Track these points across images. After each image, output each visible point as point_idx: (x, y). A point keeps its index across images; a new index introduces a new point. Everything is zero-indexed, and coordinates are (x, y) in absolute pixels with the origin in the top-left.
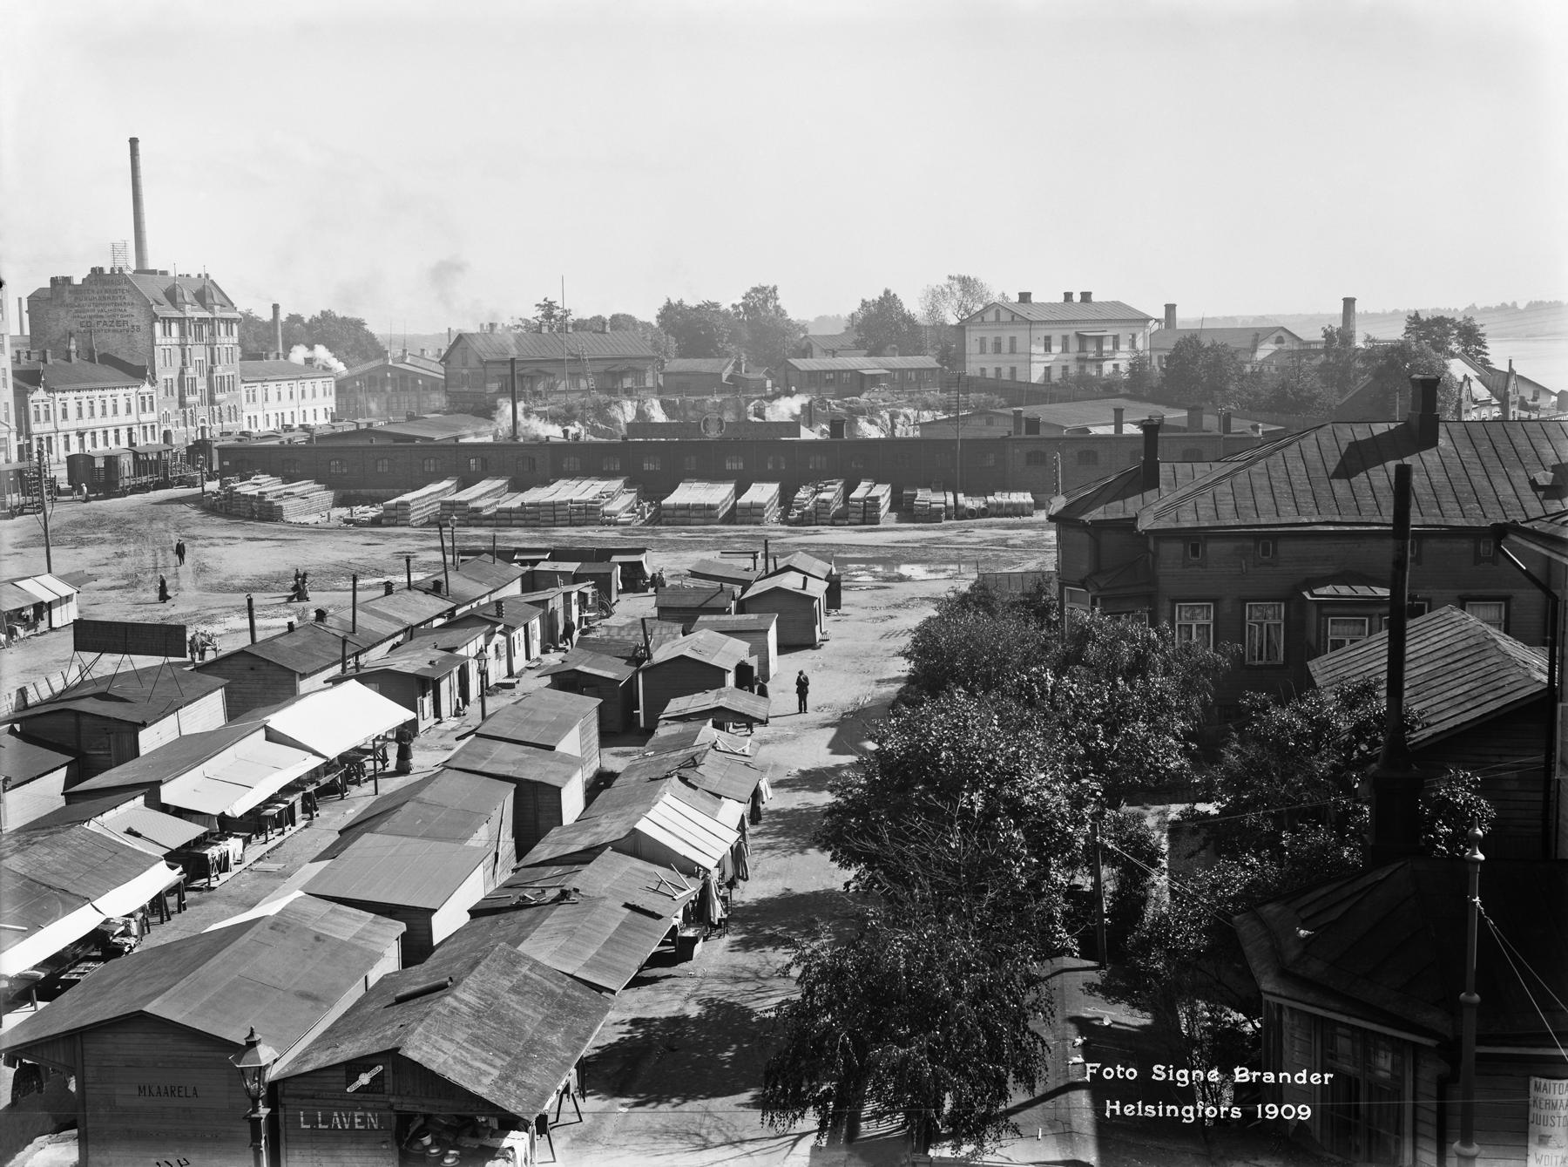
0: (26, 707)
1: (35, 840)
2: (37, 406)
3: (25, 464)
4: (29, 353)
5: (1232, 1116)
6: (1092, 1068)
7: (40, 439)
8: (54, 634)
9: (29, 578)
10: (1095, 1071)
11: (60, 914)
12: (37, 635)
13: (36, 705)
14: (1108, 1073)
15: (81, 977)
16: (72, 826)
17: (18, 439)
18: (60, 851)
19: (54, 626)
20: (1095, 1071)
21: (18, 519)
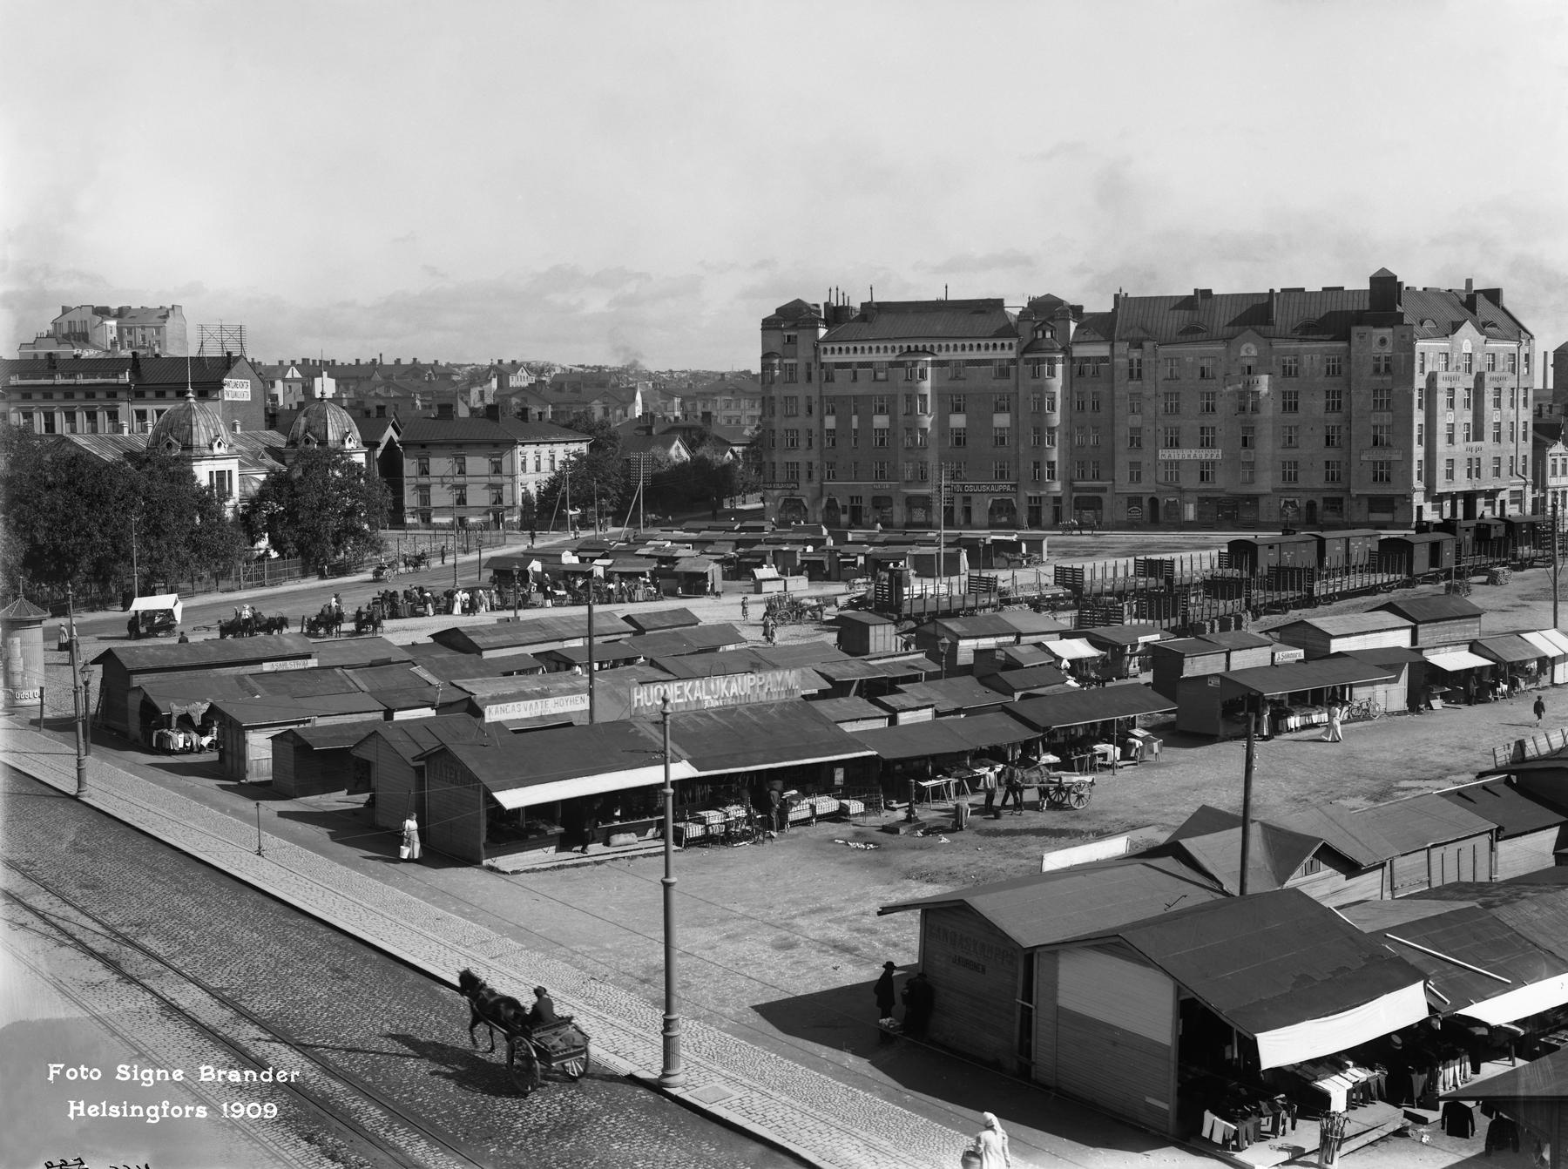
0: (1524, 760)
1: (1524, 894)
2: (1555, 460)
3: (1538, 518)
4: (1551, 406)
5: (197, 1115)
6: (55, 1069)
7: (1555, 493)
8: (1555, 690)
9: (1535, 631)
10: (58, 1072)
11: (1545, 974)
12: (1538, 689)
13: (1534, 760)
14: (95, 1074)
15: (1562, 1045)
16: (1563, 889)
17: (1533, 492)
18: (1549, 912)
19: (1556, 681)
20: (58, 1072)
21: (1528, 572)
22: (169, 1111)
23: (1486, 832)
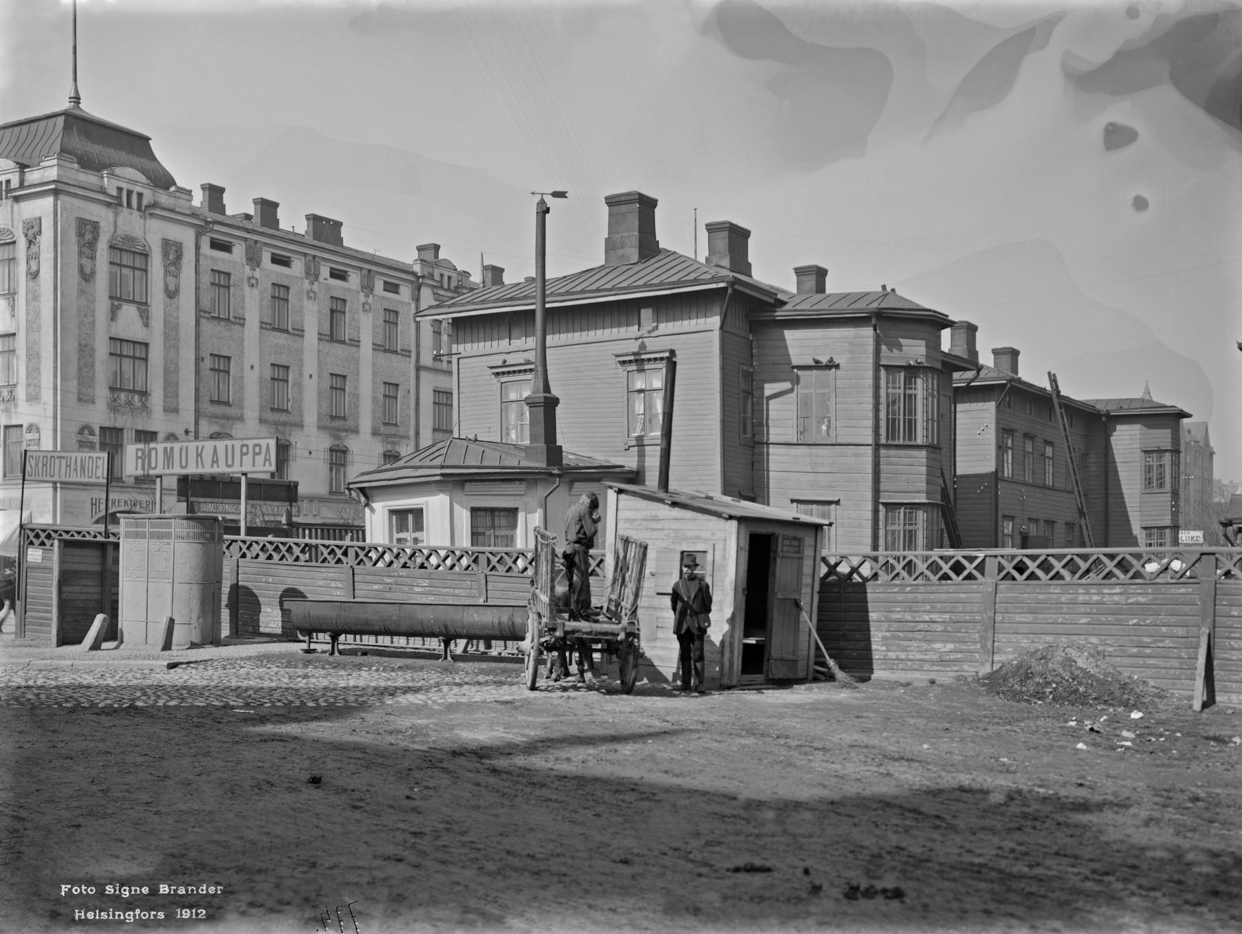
22: (139, 915)
23: (418, 378)
